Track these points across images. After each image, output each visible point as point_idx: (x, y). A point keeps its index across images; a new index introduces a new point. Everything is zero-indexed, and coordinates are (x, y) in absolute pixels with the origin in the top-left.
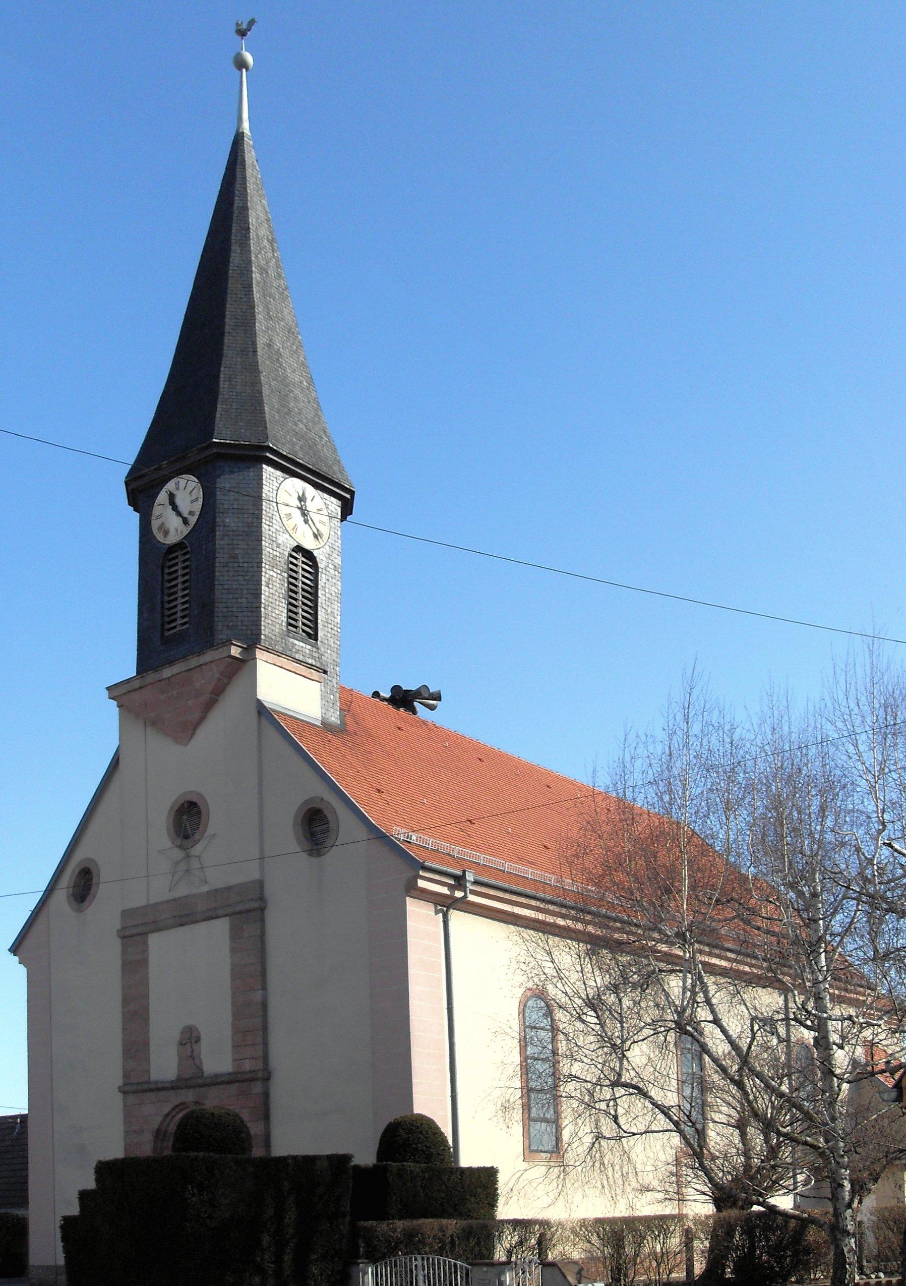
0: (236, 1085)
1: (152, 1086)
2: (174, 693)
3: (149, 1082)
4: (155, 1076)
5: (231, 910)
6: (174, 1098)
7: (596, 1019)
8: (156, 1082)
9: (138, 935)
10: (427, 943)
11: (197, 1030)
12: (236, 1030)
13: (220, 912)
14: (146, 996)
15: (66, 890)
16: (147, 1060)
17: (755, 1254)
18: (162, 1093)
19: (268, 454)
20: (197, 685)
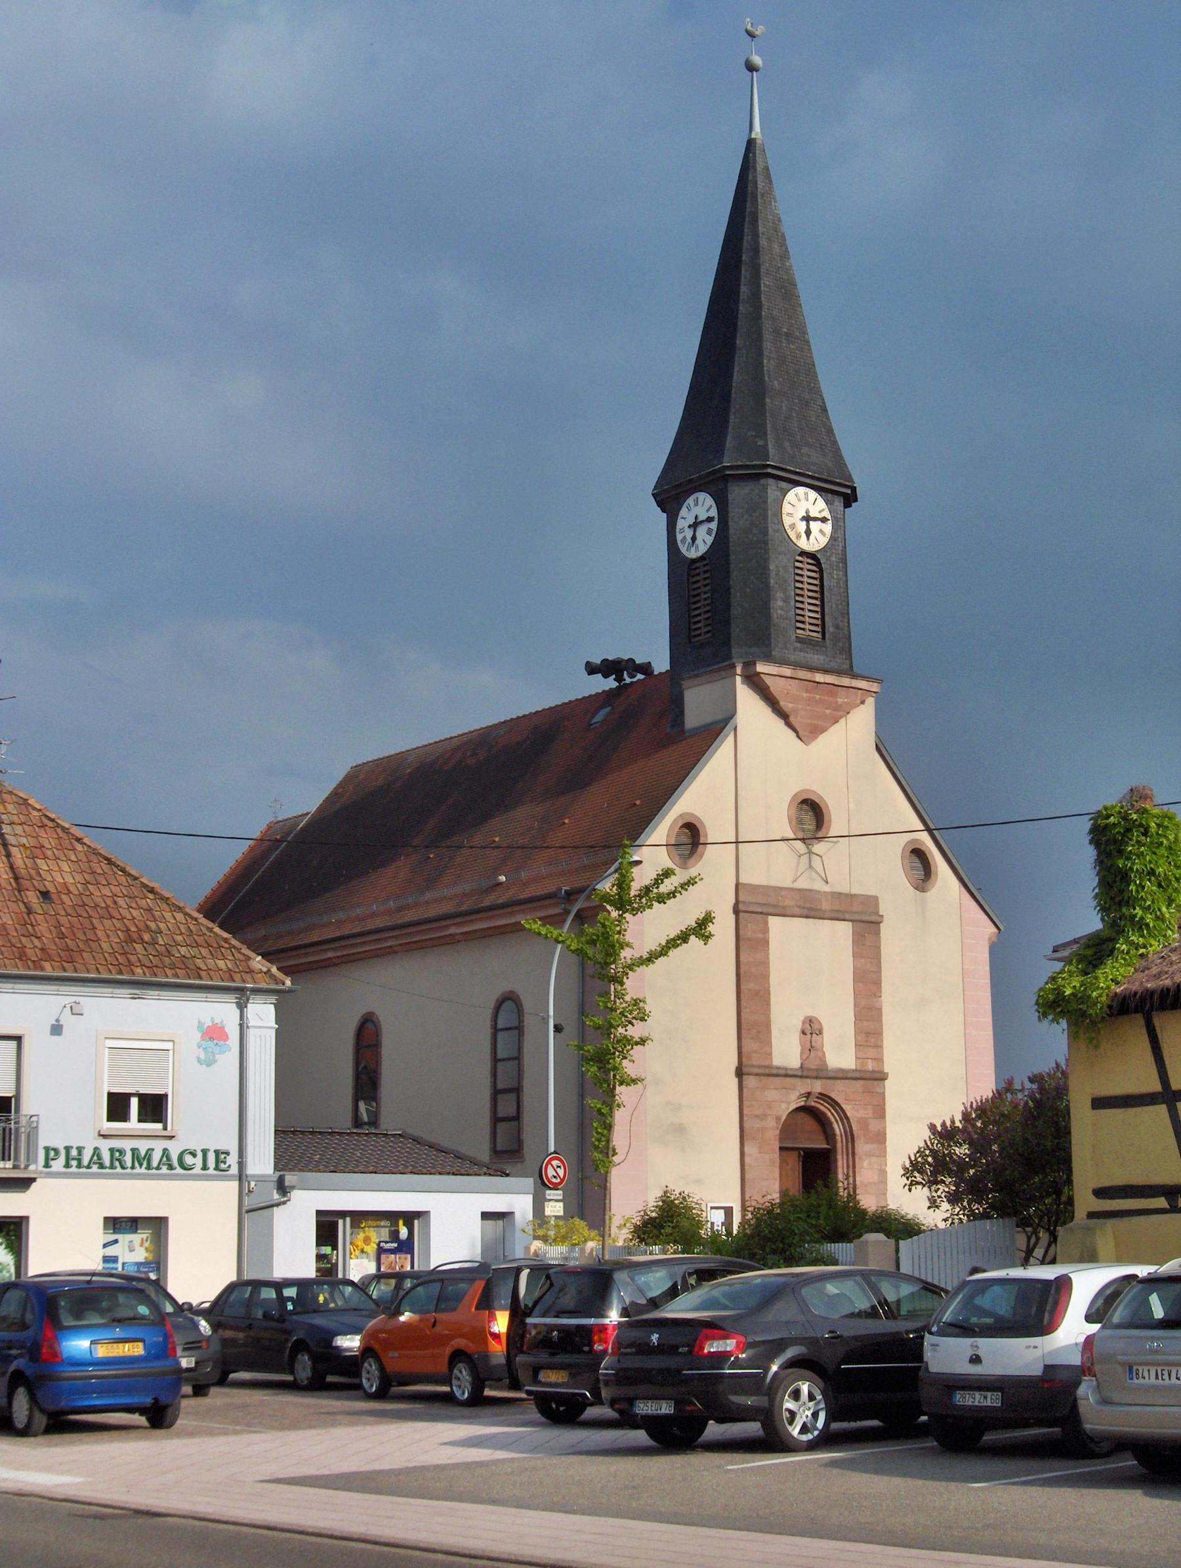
0: (862, 1082)
1: (775, 1071)
2: (818, 697)
3: (770, 1067)
4: (777, 1061)
5: (857, 917)
6: (803, 1086)
7: (1064, 1062)
8: (778, 1068)
9: (761, 913)
10: (237, 898)
11: (820, 1023)
12: (858, 1032)
13: (847, 917)
14: (766, 977)
15: (701, 842)
16: (769, 1044)
17: (944, 1230)
18: (788, 1079)
19: (727, 473)
20: (840, 701)
